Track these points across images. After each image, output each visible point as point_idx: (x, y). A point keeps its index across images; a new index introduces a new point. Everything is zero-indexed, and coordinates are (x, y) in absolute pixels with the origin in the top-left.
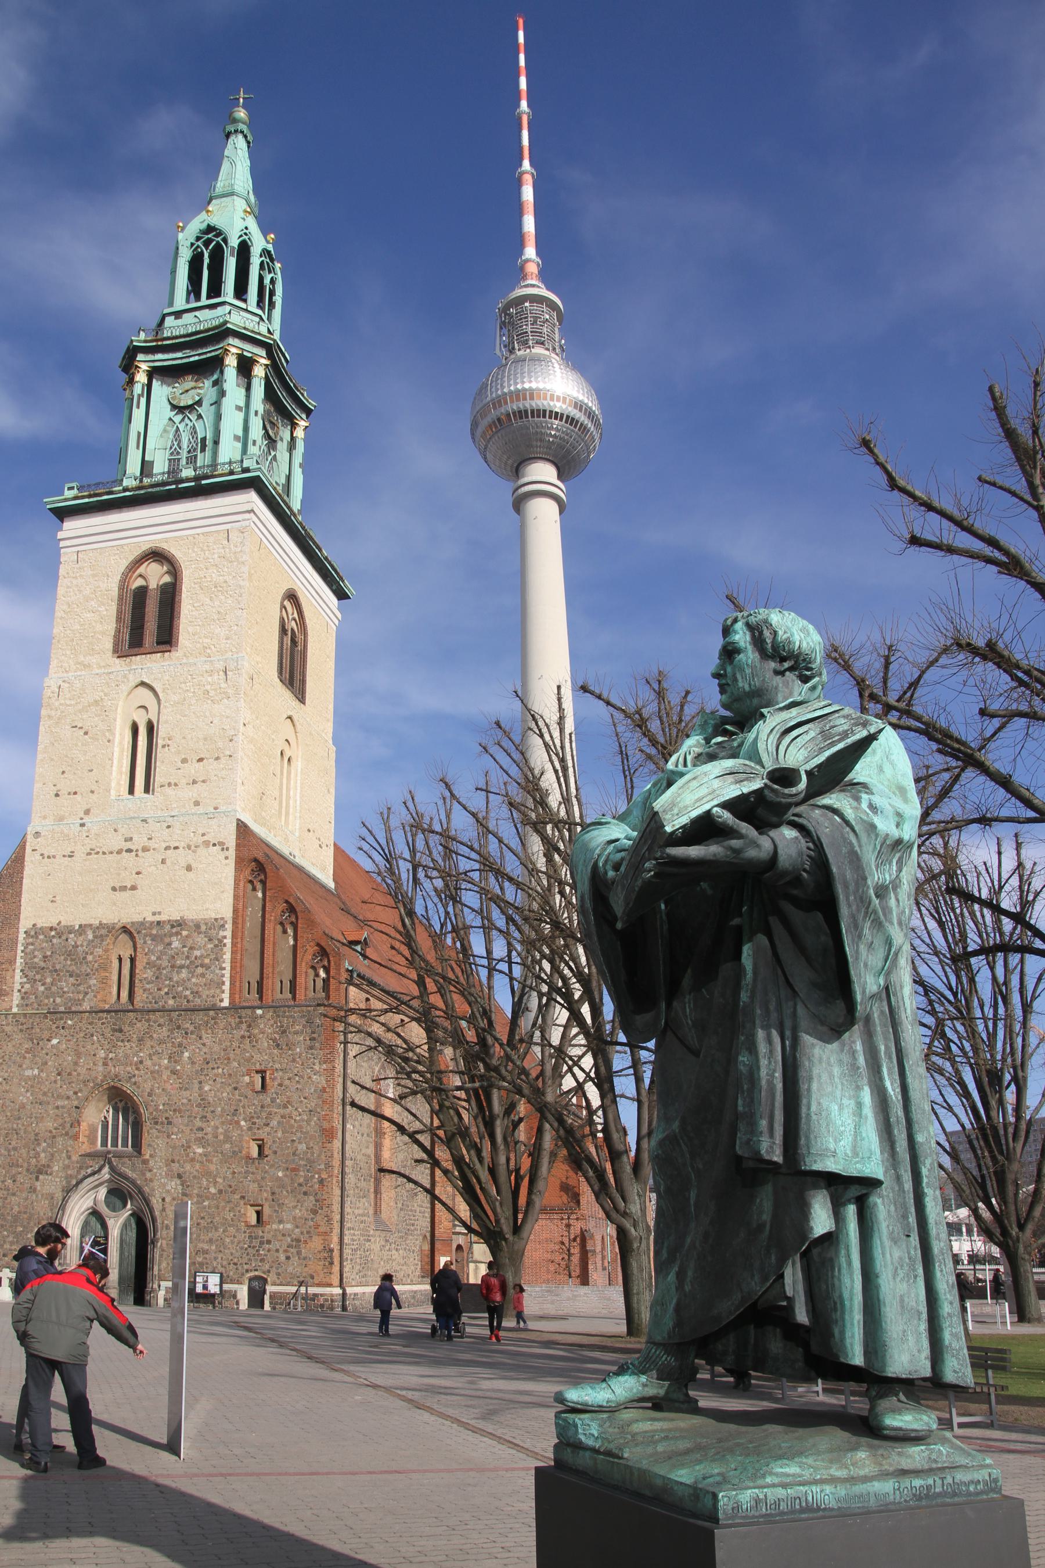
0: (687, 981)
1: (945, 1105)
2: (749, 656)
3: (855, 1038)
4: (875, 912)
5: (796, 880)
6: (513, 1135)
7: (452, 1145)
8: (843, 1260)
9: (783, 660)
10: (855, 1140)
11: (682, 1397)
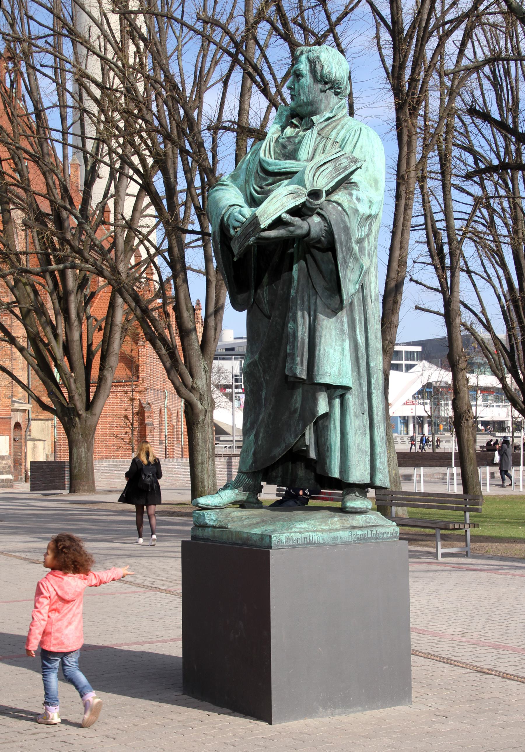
0: (265, 280)
1: (485, 275)
2: (307, 80)
3: (344, 316)
4: (355, 254)
5: (319, 241)
6: (85, 310)
7: (28, 322)
8: (332, 426)
9: (326, 83)
10: (340, 367)
11: (255, 501)
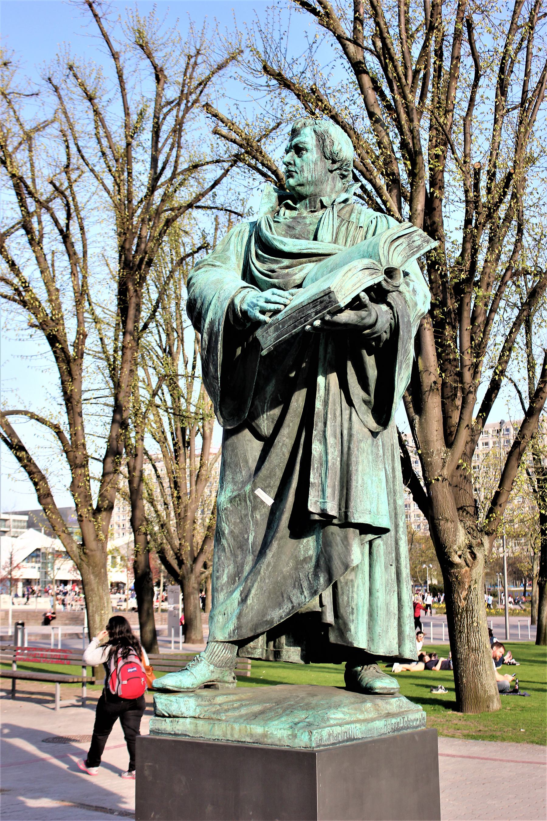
9: (334, 162)
